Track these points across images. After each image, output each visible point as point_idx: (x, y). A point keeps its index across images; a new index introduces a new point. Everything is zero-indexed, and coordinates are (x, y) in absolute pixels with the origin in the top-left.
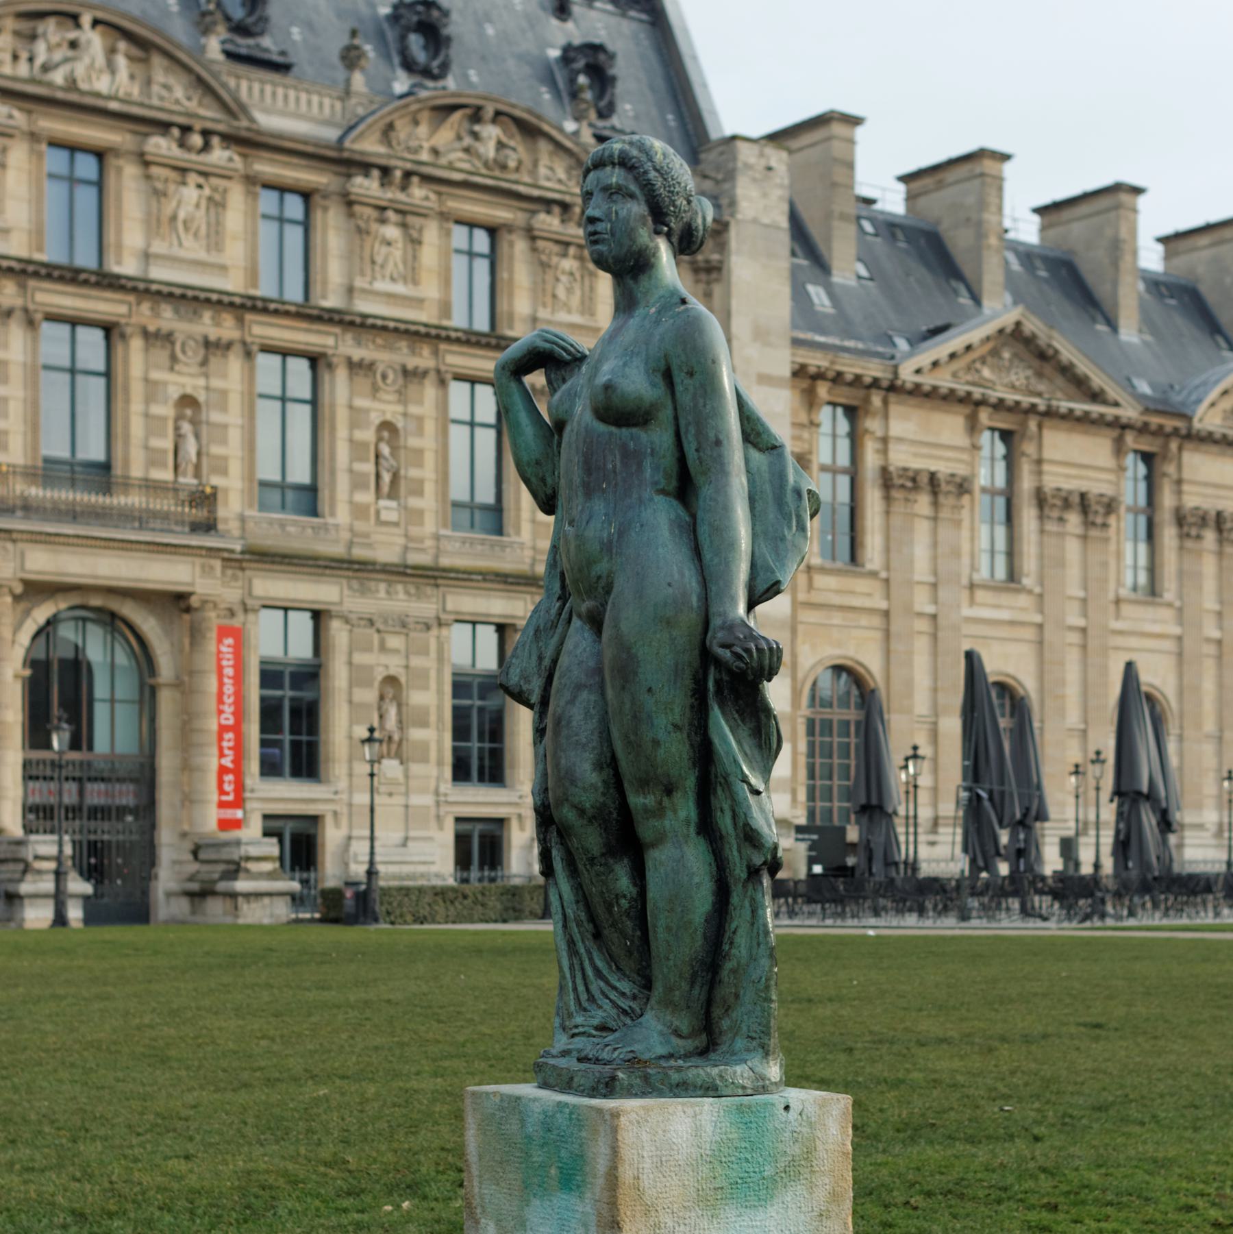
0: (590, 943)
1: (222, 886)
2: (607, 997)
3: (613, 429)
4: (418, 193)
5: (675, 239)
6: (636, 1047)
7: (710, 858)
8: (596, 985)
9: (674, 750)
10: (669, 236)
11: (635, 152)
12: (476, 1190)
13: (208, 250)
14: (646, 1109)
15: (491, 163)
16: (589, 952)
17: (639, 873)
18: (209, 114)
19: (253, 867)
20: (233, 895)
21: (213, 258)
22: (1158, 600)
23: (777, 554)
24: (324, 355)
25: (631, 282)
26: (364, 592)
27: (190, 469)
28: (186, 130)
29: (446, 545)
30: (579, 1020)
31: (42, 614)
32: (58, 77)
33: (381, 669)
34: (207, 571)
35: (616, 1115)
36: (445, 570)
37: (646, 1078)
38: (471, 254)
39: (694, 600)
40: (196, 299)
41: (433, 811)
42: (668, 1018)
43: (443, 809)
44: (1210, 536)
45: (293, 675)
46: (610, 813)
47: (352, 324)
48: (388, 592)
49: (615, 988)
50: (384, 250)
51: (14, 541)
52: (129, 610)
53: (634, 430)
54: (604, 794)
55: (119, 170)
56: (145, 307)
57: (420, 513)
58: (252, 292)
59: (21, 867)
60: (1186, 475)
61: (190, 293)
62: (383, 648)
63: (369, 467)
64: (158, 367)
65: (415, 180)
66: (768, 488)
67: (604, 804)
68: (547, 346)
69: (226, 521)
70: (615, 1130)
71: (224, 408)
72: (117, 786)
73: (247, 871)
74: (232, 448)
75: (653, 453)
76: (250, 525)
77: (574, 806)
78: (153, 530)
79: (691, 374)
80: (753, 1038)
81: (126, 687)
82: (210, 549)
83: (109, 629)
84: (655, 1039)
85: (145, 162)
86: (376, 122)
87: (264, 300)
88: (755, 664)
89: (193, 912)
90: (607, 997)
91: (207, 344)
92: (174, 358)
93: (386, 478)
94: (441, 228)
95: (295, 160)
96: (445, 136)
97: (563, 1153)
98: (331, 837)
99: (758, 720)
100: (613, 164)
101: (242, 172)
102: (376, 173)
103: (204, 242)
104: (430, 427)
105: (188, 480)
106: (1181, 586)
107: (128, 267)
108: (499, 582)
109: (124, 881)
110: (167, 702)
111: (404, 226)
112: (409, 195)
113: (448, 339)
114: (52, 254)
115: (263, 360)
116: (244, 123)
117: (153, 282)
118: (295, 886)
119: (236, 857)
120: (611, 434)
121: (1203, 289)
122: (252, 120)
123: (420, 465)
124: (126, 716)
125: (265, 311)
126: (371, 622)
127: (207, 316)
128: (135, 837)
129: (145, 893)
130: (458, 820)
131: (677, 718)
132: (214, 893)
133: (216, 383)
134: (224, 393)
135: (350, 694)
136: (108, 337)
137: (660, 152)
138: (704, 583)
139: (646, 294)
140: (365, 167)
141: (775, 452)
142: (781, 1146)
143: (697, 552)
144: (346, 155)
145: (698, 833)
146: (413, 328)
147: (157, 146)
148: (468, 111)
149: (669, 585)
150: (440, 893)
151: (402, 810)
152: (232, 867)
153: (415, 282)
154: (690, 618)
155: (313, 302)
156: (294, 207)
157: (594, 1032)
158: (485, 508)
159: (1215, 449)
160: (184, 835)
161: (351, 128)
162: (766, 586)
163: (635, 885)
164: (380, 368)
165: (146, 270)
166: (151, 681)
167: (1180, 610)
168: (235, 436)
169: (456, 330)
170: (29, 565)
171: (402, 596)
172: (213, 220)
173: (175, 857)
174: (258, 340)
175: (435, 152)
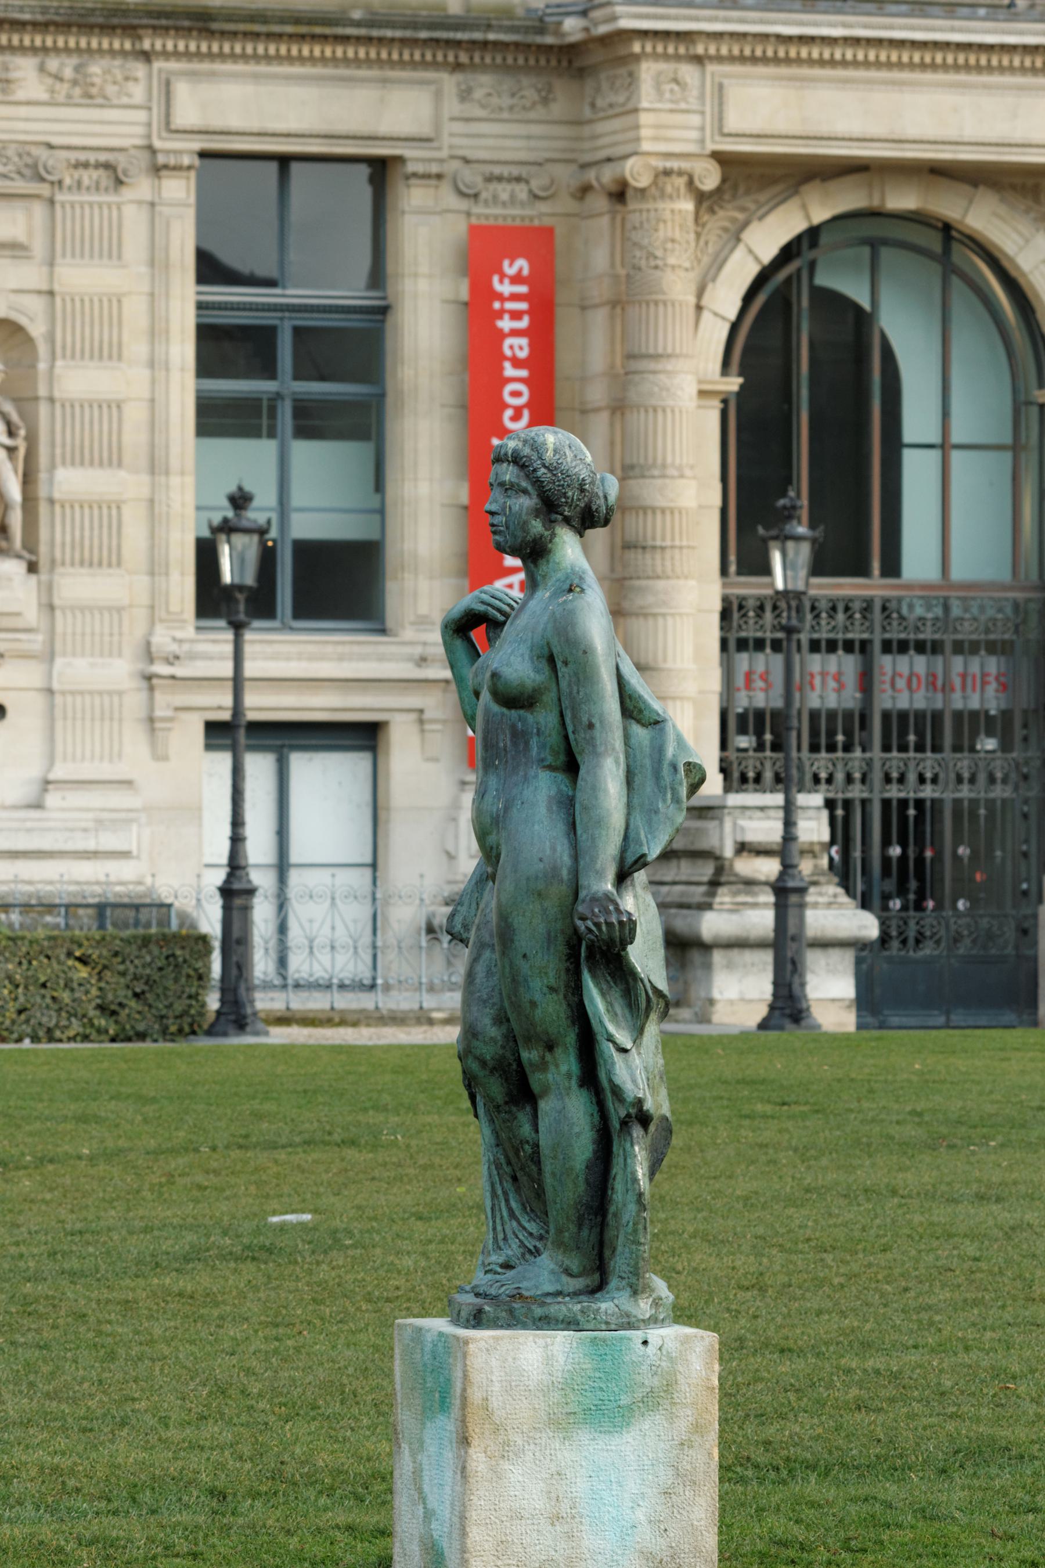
3: (505, 710)
6: (524, 1284)
7: (595, 1109)
9: (551, 1010)
10: (567, 521)
11: (527, 451)
14: (497, 1339)
16: (505, 1193)
35: (466, 1342)
37: (511, 1312)
39: (565, 873)
42: (560, 1257)
46: (510, 1064)
49: (524, 1228)
51: (699, 60)
53: (522, 712)
54: (503, 1047)
59: (706, 871)
66: (647, 762)
67: (503, 1057)
68: (482, 608)
72: (958, 663)
77: (476, 1058)
79: (566, 663)
80: (622, 1278)
83: (936, 268)
99: (627, 983)
109: (974, 901)
120: (503, 714)
128: (999, 792)
137: (551, 446)
138: (576, 857)
139: (544, 577)
141: (658, 727)
142: (638, 1378)
143: (573, 826)
145: (581, 1086)
149: (541, 860)
154: (559, 891)
157: (499, 1270)
162: (634, 859)
170: (734, 122)
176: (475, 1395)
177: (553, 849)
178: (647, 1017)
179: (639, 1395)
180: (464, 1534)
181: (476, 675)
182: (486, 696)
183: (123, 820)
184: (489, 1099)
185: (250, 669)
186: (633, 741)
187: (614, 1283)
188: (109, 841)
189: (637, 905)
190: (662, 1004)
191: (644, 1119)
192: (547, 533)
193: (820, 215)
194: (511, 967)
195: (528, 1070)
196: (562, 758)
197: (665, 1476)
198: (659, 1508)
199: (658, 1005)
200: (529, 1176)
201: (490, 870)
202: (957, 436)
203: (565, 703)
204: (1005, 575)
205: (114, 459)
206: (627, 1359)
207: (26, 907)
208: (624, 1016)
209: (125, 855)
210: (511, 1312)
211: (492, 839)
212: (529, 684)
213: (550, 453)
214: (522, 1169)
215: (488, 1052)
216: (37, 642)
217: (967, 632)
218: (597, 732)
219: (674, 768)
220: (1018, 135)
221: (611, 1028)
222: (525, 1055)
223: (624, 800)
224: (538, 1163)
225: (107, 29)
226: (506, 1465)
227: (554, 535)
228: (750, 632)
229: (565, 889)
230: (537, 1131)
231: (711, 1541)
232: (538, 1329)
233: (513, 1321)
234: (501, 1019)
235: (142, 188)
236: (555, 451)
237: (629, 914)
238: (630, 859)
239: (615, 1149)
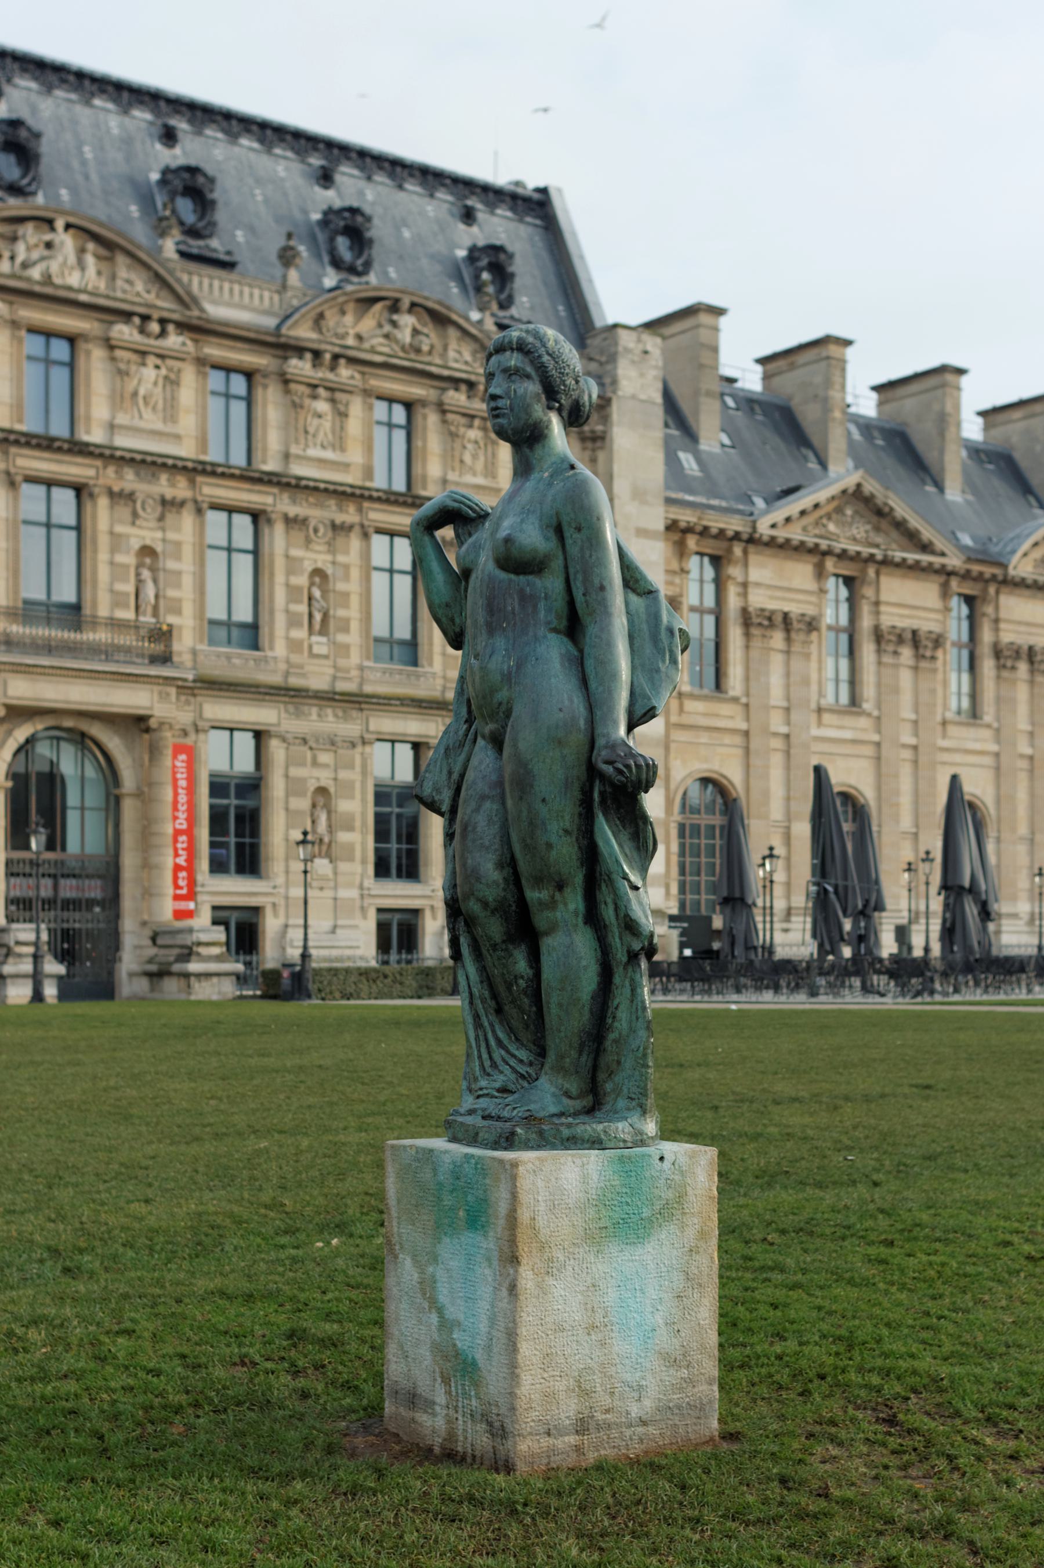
0: (493, 1017)
1: (177, 967)
2: (507, 1064)
3: (512, 576)
4: (345, 373)
6: (532, 1107)
7: (595, 944)
8: (498, 1054)
10: (559, 411)
11: (530, 339)
12: (395, 1229)
16: (492, 1025)
17: (535, 958)
18: (165, 305)
19: (203, 951)
20: (187, 975)
21: (169, 428)
22: (978, 722)
23: (653, 684)
24: (264, 512)
25: (527, 451)
26: (298, 714)
27: (149, 610)
28: (145, 318)
29: (369, 675)
30: (483, 1083)
31: (22, 734)
32: (36, 273)
33: (313, 781)
34: (164, 697)
35: (515, 1165)
36: (368, 696)
38: (390, 426)
39: (582, 723)
40: (154, 463)
41: (358, 903)
42: (560, 1081)
44: (1023, 667)
45: (237, 786)
48: (319, 715)
49: (514, 1056)
50: (316, 421)
52: (97, 731)
53: (530, 577)
54: (504, 890)
55: (88, 353)
56: (111, 471)
57: (347, 647)
58: (202, 458)
60: (1003, 615)
61: (149, 459)
62: (315, 763)
63: (303, 608)
64: (121, 522)
65: (342, 361)
66: (645, 627)
67: (505, 898)
68: (456, 505)
69: (180, 654)
70: (514, 1178)
71: (178, 557)
72: (87, 882)
73: (198, 954)
74: (186, 592)
75: (546, 598)
76: (201, 658)
77: (479, 900)
78: (118, 662)
80: (632, 1099)
81: (94, 797)
82: (166, 678)
84: (548, 1099)
85: (110, 345)
87: (213, 464)
89: (152, 989)
90: (507, 1064)
92: (135, 515)
93: (318, 617)
94: (364, 402)
95: (239, 345)
96: (368, 324)
97: (470, 1198)
98: (271, 925)
99: (637, 826)
100: (512, 349)
101: (194, 355)
102: (308, 356)
103: (161, 415)
104: (355, 573)
105: (147, 619)
106: (998, 710)
107: (95, 436)
110: (129, 807)
111: (333, 401)
112: (337, 375)
113: (371, 498)
116: (196, 313)
117: (117, 449)
118: (240, 967)
119: (189, 943)
120: (510, 580)
121: (1017, 456)
122: (202, 310)
124: (94, 821)
125: (213, 474)
126: (305, 741)
127: (164, 478)
128: (102, 926)
129: (111, 973)
130: (380, 910)
132: (170, 974)
133: (171, 536)
134: (178, 544)
135: (287, 802)
136: (78, 496)
138: (591, 709)
140: (299, 351)
142: (656, 1191)
144: (283, 340)
145: (585, 923)
147: (121, 332)
148: (387, 303)
150: (365, 973)
151: (331, 902)
152: (186, 951)
153: (343, 449)
154: (578, 738)
156: (238, 385)
158: (402, 643)
159: (1027, 592)
160: (144, 924)
161: (287, 317)
163: (531, 967)
164: (312, 523)
166: (116, 792)
167: (998, 730)
168: (187, 581)
169: (377, 490)
170: (11, 692)
171: (331, 718)
172: (169, 396)
174: (207, 499)
175: (359, 337)
180: (513, 1348)
197: (678, 1281)
198: (673, 1311)
210: (541, 1133)
226: (551, 1281)
228: (15, 870)
231: (713, 1338)
232: (567, 1149)
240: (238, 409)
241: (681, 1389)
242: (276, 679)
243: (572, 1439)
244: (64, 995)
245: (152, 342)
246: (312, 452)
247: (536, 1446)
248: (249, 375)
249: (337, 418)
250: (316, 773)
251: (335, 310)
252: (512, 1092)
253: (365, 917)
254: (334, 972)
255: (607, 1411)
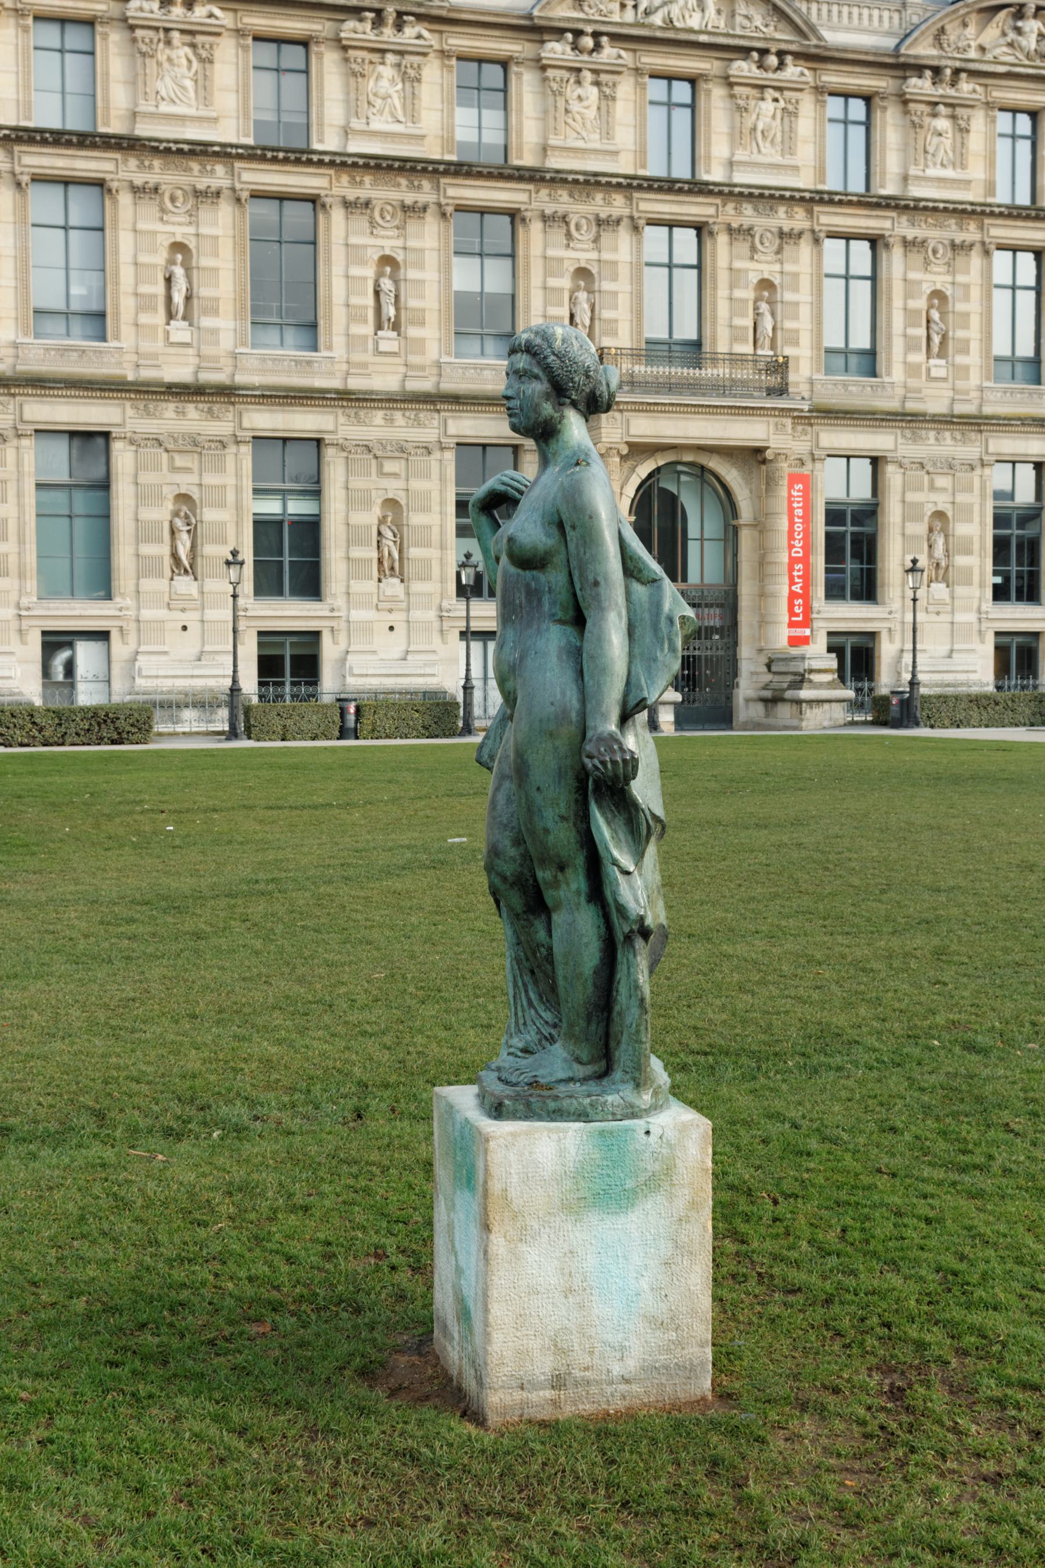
1: (789, 694)
3: (520, 571)
4: (966, 87)
5: (582, 406)
6: (541, 1072)
9: (562, 836)
10: (574, 404)
11: (538, 341)
13: (782, 156)
14: (514, 1135)
15: (1032, 53)
16: (525, 985)
18: (783, 36)
19: (816, 678)
20: (799, 702)
21: (788, 161)
23: (649, 673)
24: (882, 236)
26: (915, 439)
27: (767, 342)
28: (764, 52)
29: (989, 396)
31: (644, 469)
32: (657, 19)
33: (930, 505)
34: (779, 428)
36: (987, 417)
37: (528, 1105)
38: (1014, 137)
39: (574, 715)
40: (772, 196)
41: (976, 627)
43: (984, 625)
45: (854, 514)
47: (906, 207)
48: (937, 439)
50: (936, 140)
52: (714, 463)
53: (535, 572)
54: (521, 865)
55: (708, 92)
56: (730, 207)
57: (966, 368)
58: (820, 187)
61: (767, 192)
62: (932, 488)
63: (922, 332)
64: (740, 258)
65: (963, 75)
66: (646, 616)
67: (521, 873)
68: (503, 488)
69: (797, 384)
71: (796, 289)
72: (706, 610)
73: (810, 681)
74: (803, 323)
75: (550, 591)
76: (818, 387)
77: (498, 874)
78: (735, 396)
81: (713, 527)
82: (782, 409)
84: (559, 1064)
85: (729, 83)
86: (928, 28)
87: (830, 193)
88: (610, 774)
89: (767, 716)
91: (781, 234)
92: (753, 249)
93: (936, 339)
94: (987, 116)
95: (857, 69)
96: (991, 34)
98: (887, 651)
99: (630, 813)
101: (812, 84)
102: (928, 73)
103: (779, 148)
104: (975, 293)
105: (765, 351)
107: (715, 174)
108: (1036, 426)
110: (746, 538)
111: (953, 117)
112: (957, 90)
113: (992, 214)
114: (655, 169)
115: (829, 244)
116: (814, 42)
117: (736, 186)
118: (850, 694)
119: (801, 671)
122: (820, 38)
123: (966, 326)
124: (713, 554)
125: (831, 202)
126: (922, 466)
127: (782, 210)
128: (720, 653)
129: (729, 698)
130: (998, 634)
131: (563, 809)
132: (783, 700)
133: (788, 267)
134: (796, 275)
135: (903, 527)
136: (699, 236)
137: (559, 337)
138: (583, 700)
139: (554, 454)
140: (918, 69)
142: (642, 1165)
143: (580, 673)
144: (902, 60)
146: (960, 207)
147: (739, 68)
148: (1012, 9)
149: (552, 704)
150: (977, 701)
151: (949, 626)
152: (798, 678)
153: (963, 167)
154: (567, 732)
155: (873, 192)
156: (857, 109)
158: (1026, 361)
160: (761, 650)
161: (907, 36)
164: (931, 244)
165: (730, 177)
166: (734, 522)
168: (805, 312)
169: (999, 206)
170: (632, 432)
171: (949, 441)
172: (787, 128)
173: (752, 669)
174: (824, 228)
175: (982, 49)
176: (496, 1187)
177: (563, 694)
178: (648, 842)
179: (642, 1179)
181: (497, 543)
182: (504, 559)
183: (433, 663)
184: (511, 909)
185: (472, 614)
186: (634, 597)
187: (617, 1075)
188: (428, 671)
189: (637, 742)
190: (659, 828)
191: (645, 933)
192: (556, 415)
193: (661, 463)
194: (527, 799)
195: (542, 887)
196: (571, 613)
197: (665, 1248)
198: (660, 1277)
199: (656, 829)
200: (545, 973)
201: (509, 711)
202: (706, 536)
203: (574, 563)
204: (722, 582)
205: (429, 545)
206: (631, 1148)
207: (400, 693)
208: (627, 842)
209: (433, 675)
210: (528, 1105)
211: (509, 685)
212: (541, 547)
213: (559, 343)
214: (539, 967)
215: (509, 869)
216: (404, 605)
217: (709, 601)
218: (602, 589)
219: (671, 620)
220: (726, 436)
221: (616, 853)
222: (540, 874)
223: (627, 649)
224: (552, 963)
225: (425, 402)
226: (524, 1248)
227: (562, 417)
229: (573, 730)
230: (551, 936)
231: (705, 1303)
233: (529, 1114)
234: (518, 841)
235: (437, 455)
236: (563, 341)
237: (632, 752)
238: (632, 702)
239: (619, 956)
240: (857, 134)
241: (668, 1351)
242: (893, 405)
243: (548, 1394)
244: (680, 722)
245: (770, 75)
246: (931, 172)
247: (508, 1398)
248: (868, 99)
249: (958, 135)
250: (933, 497)
251: (957, 23)
252: (532, 1053)
253: (983, 642)
254: (943, 698)
255: (586, 1369)
